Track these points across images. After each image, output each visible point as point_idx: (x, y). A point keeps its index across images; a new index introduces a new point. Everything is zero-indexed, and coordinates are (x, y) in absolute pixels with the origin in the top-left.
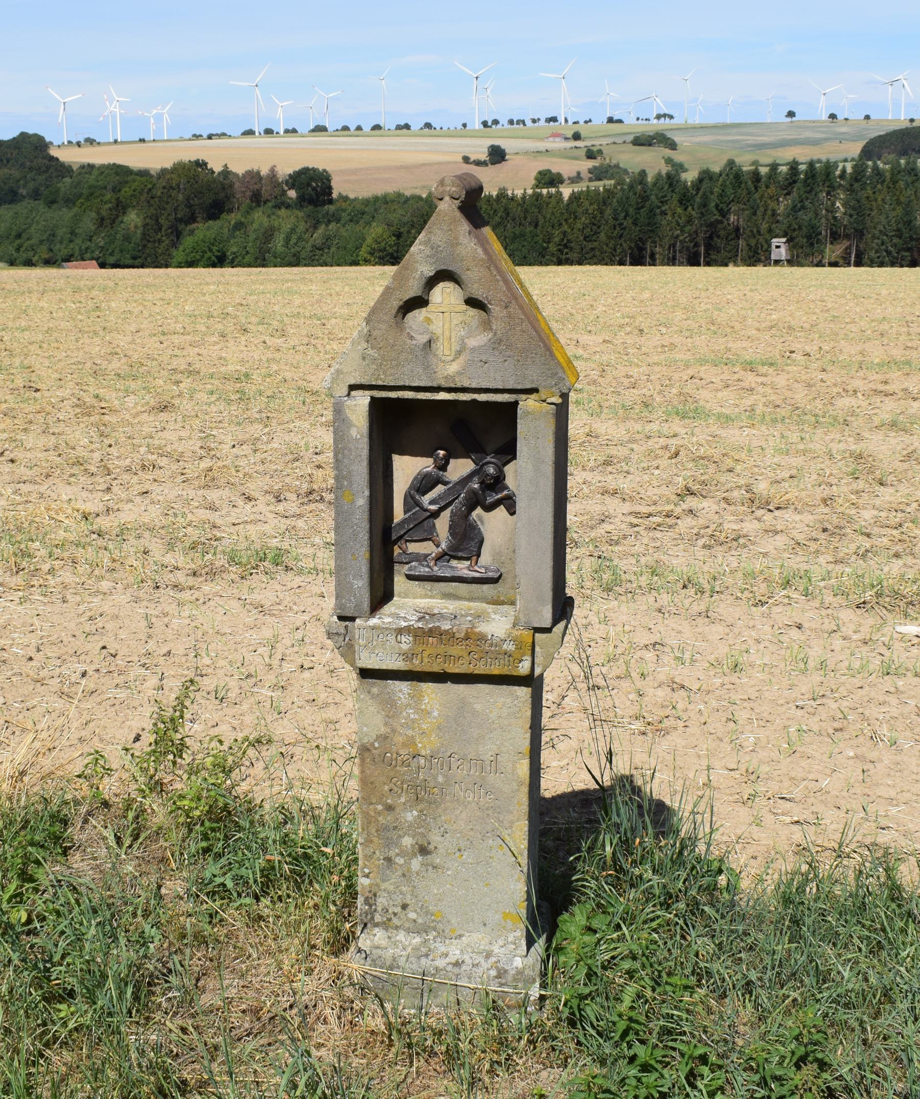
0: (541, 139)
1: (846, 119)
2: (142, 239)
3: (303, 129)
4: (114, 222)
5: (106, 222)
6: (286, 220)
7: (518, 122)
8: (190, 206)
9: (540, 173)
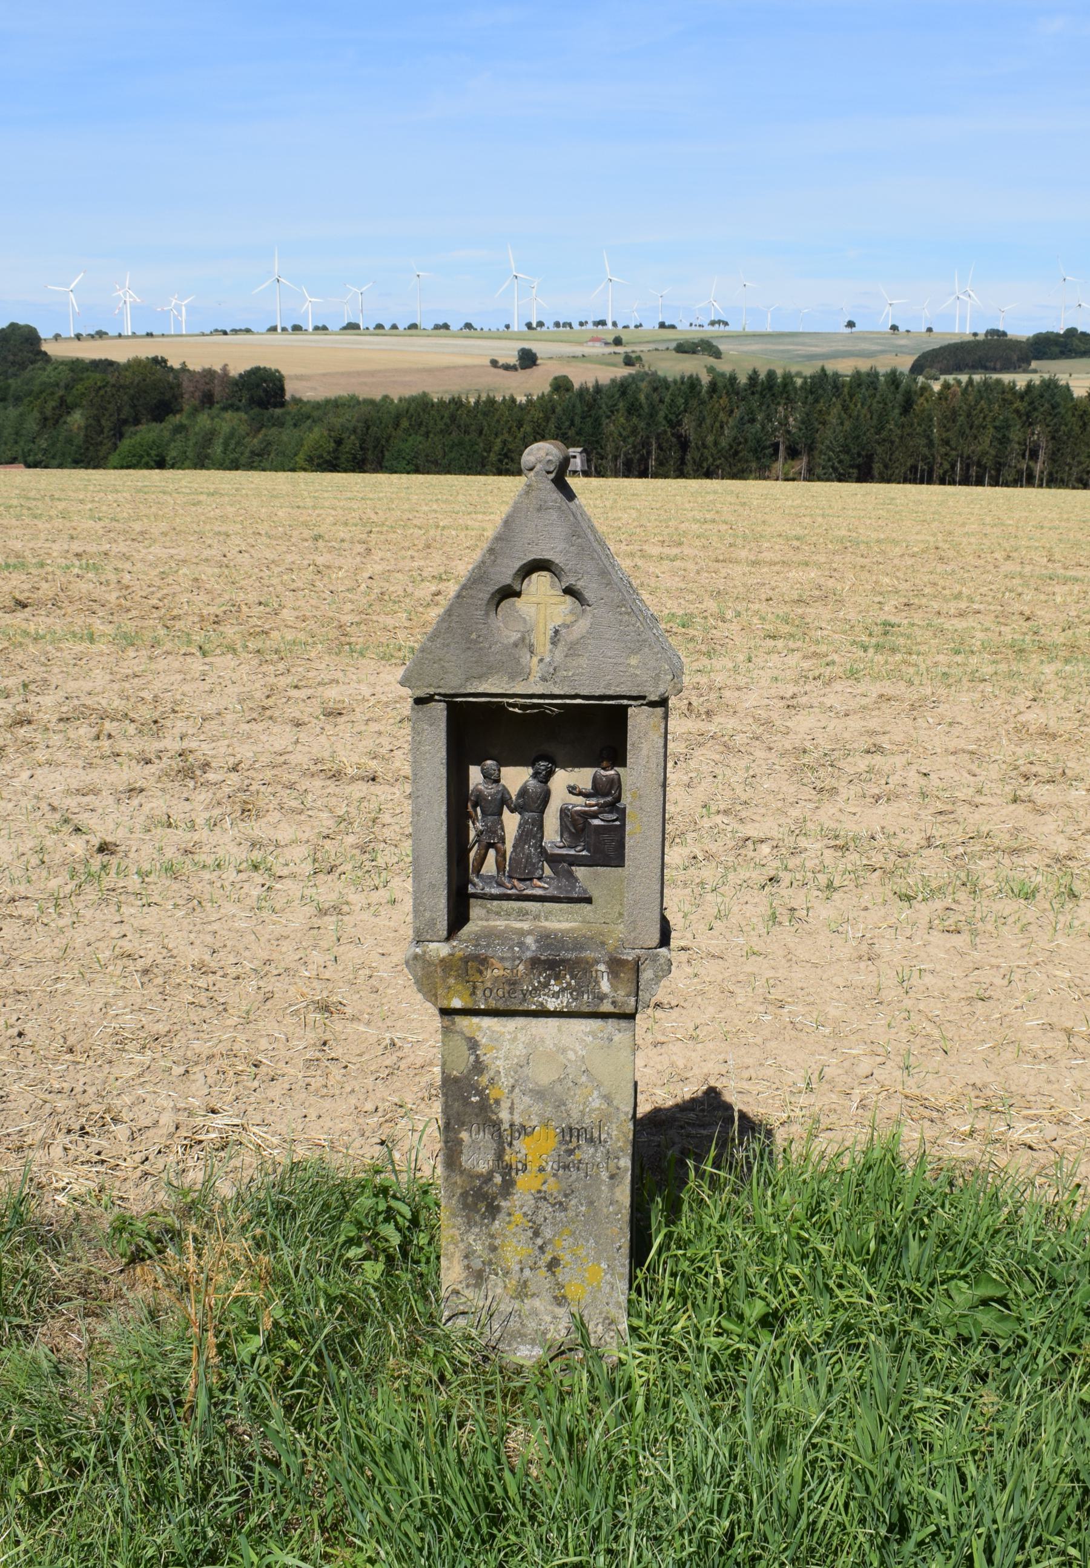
0: (580, 343)
2: (86, 441)
3: (334, 326)
4: (57, 422)
5: (51, 421)
6: (229, 422)
7: (565, 325)
8: (134, 406)
9: (556, 379)
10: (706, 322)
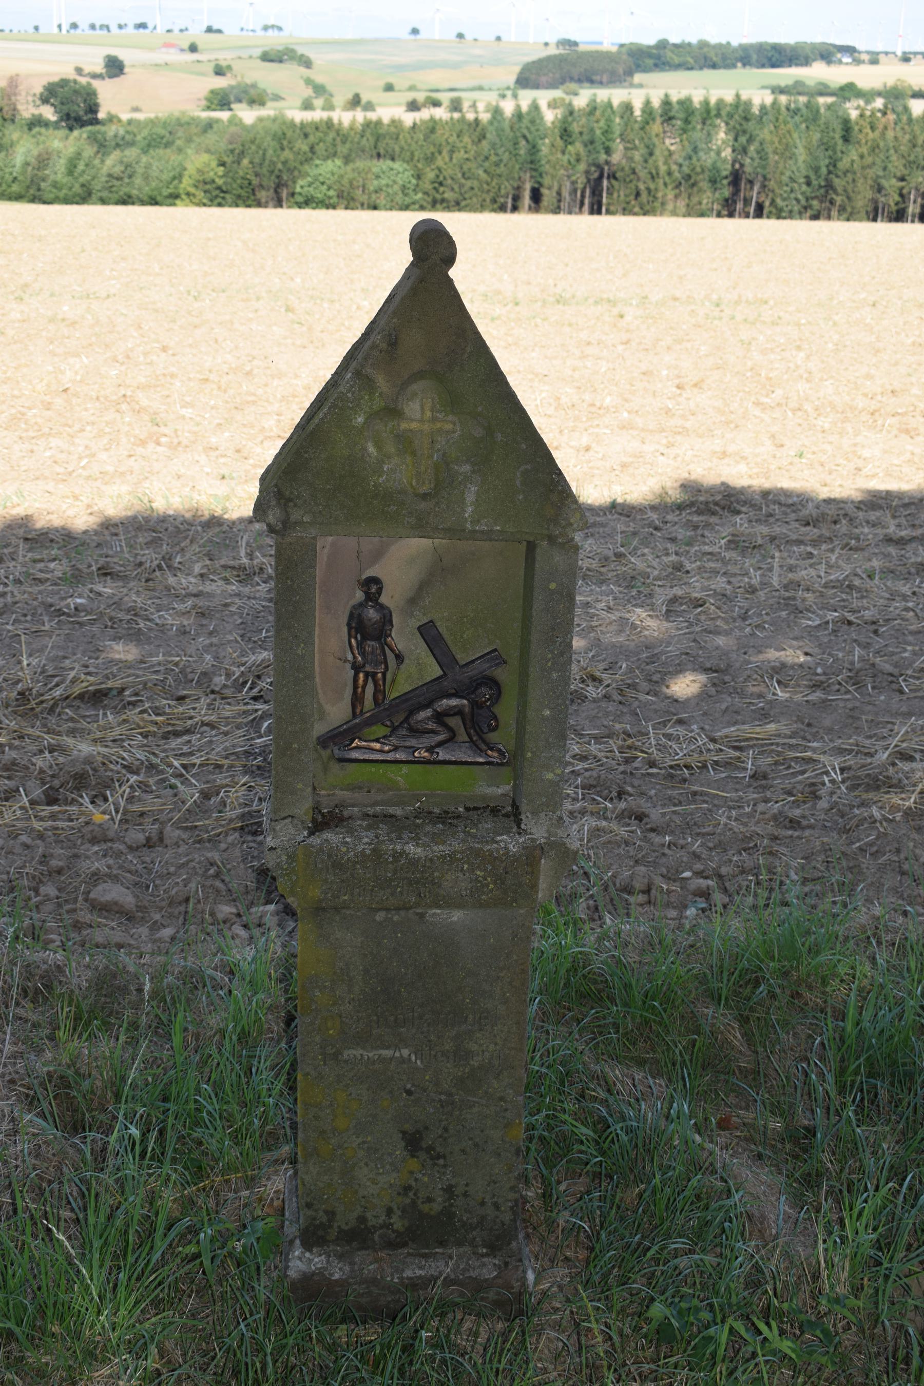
1: (476, 40)
7: (102, 27)
10: (258, 28)
